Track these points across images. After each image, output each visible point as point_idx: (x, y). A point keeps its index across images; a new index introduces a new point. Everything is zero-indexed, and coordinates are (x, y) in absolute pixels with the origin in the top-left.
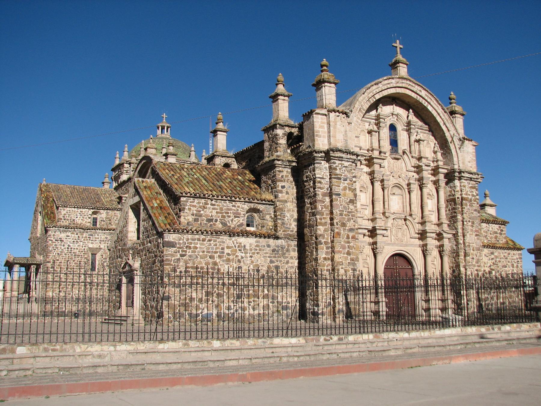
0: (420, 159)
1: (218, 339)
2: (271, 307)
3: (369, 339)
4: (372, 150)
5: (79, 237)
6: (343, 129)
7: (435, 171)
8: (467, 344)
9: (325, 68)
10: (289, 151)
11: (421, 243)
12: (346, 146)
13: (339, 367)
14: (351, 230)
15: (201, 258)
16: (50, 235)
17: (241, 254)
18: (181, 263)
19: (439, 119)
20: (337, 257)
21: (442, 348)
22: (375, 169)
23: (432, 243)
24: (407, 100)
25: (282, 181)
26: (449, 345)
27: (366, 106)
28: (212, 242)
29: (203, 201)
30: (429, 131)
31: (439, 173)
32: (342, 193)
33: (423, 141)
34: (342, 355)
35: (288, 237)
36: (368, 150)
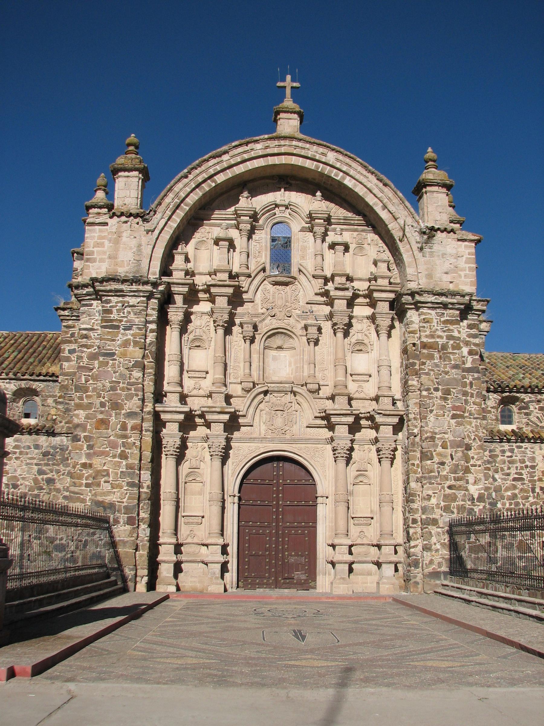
6: (133, 243)
24: (275, 172)
25: (70, 342)
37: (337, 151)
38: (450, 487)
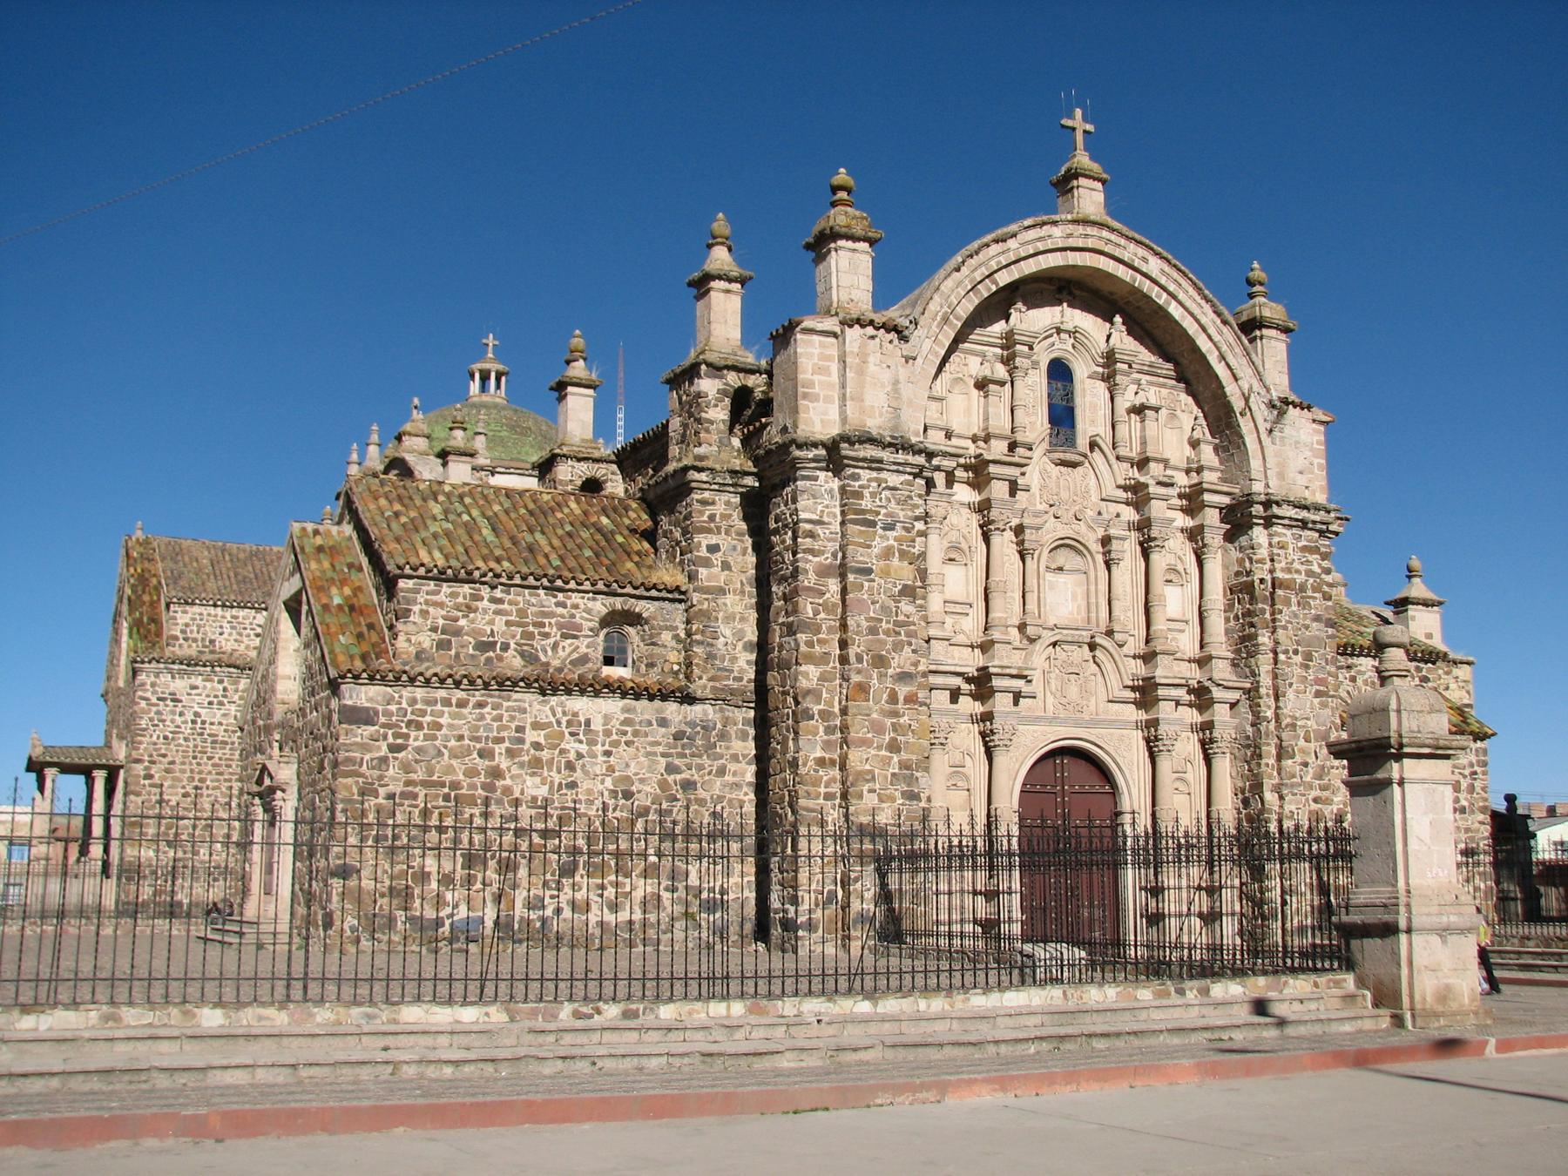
0: (1142, 463)
1: (220, 1004)
2: (667, 903)
3: (728, 1016)
4: (987, 439)
5: (225, 689)
6: (886, 376)
7: (1193, 501)
8: (1062, 1038)
9: (843, 195)
10: (736, 442)
11: (1142, 716)
12: (895, 428)
13: (530, 1104)
14: (904, 677)
15: (454, 756)
16: (143, 684)
17: (577, 745)
18: (391, 772)
19: (1203, 344)
20: (856, 758)
21: (971, 1049)
22: (994, 495)
23: (1177, 718)
24: (1106, 288)
25: (709, 531)
26: (997, 1042)
27: (967, 307)
28: (488, 709)
29: (466, 589)
30: (1178, 381)
31: (1203, 506)
32: (876, 565)
33: (1157, 410)
34: (609, 1064)
35: (722, 698)
36: (974, 439)
37: (1162, 258)
38: (1316, 800)
